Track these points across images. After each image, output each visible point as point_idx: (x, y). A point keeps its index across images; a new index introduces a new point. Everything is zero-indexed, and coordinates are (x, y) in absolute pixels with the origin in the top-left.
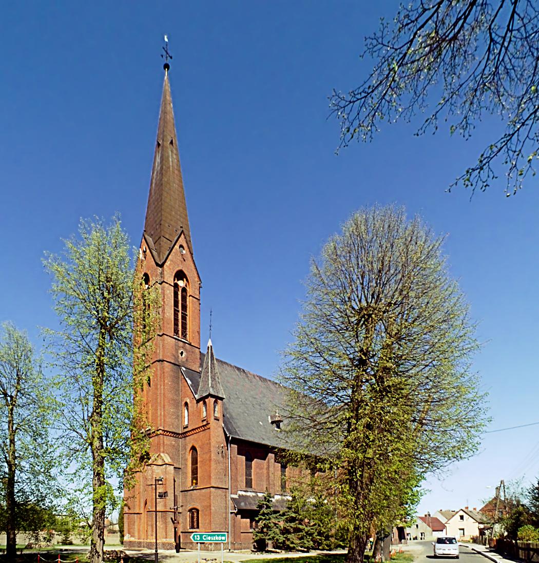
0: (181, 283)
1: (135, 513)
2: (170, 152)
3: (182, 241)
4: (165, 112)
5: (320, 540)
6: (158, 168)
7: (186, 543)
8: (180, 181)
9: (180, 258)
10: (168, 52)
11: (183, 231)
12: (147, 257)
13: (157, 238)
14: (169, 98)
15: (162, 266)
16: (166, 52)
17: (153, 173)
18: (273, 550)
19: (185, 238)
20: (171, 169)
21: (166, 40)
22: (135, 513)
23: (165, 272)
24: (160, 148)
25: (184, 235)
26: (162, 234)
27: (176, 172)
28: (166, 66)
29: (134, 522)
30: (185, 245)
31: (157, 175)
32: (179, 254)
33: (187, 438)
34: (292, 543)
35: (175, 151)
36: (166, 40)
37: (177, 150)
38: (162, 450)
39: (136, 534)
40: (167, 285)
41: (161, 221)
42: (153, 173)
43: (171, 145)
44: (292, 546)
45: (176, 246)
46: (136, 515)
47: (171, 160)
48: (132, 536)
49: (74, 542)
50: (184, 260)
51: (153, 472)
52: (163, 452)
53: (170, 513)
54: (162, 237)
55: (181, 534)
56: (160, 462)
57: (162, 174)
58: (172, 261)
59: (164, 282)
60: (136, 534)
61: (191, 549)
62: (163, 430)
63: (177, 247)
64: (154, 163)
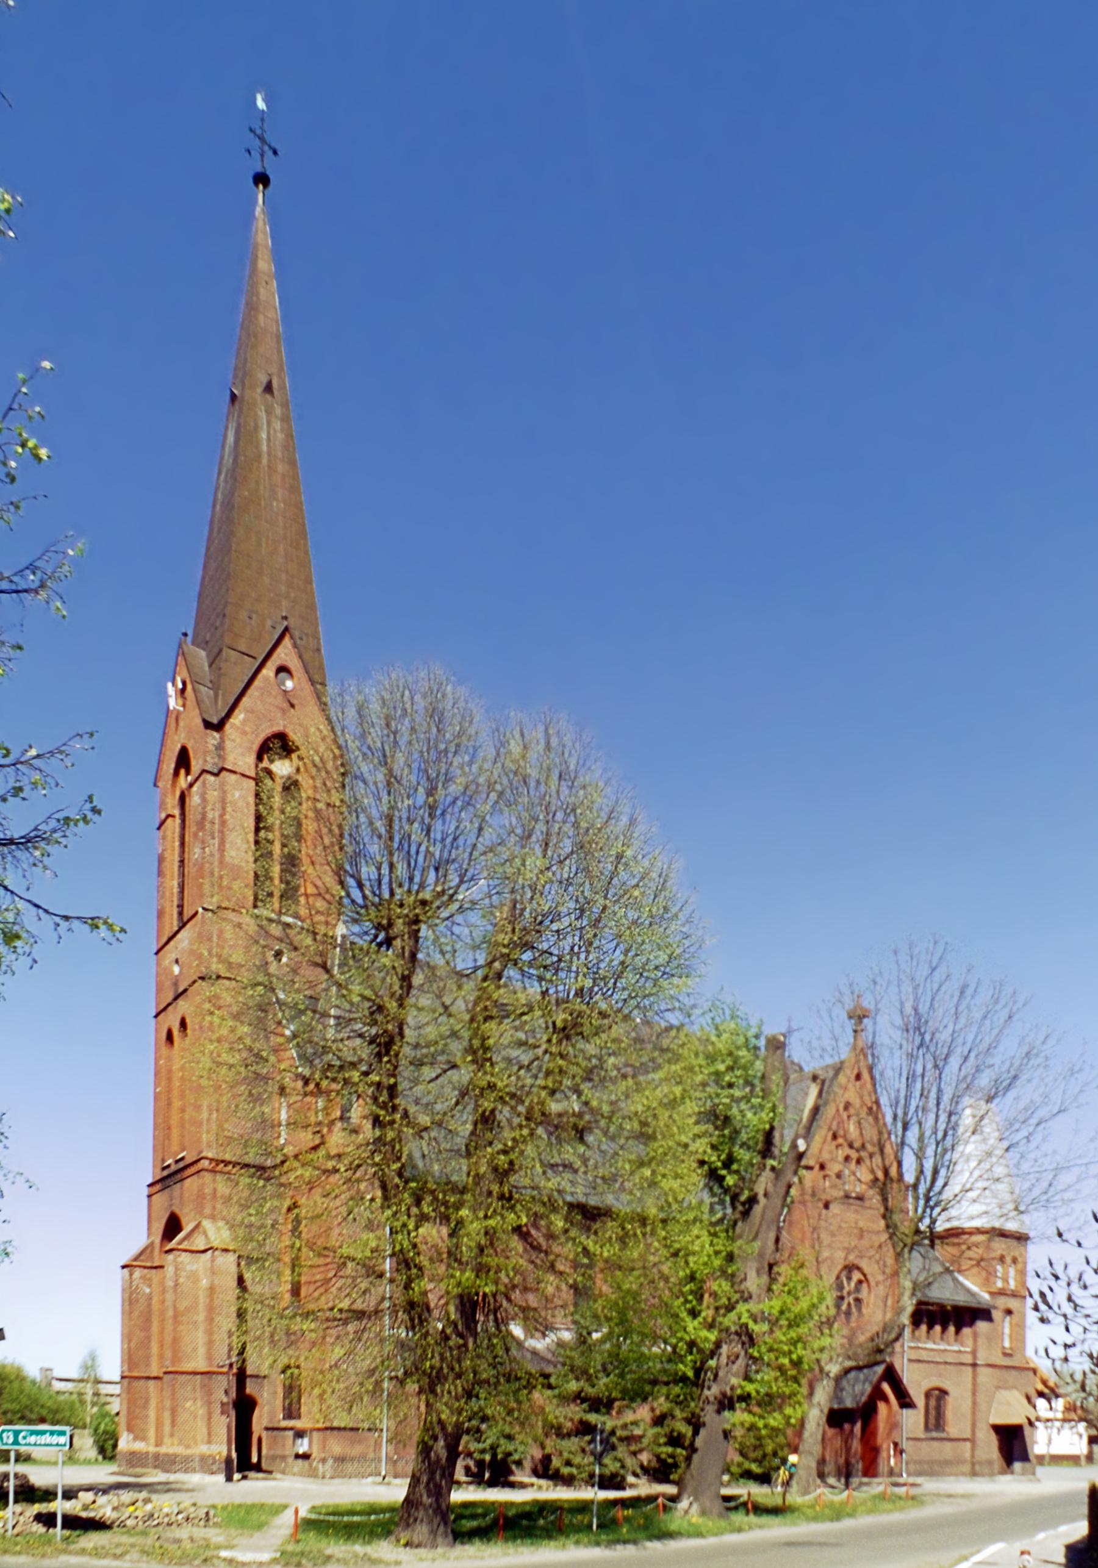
0: (282, 768)
1: (148, 1378)
2: (263, 415)
3: (285, 654)
4: (252, 308)
5: (672, 1456)
6: (228, 461)
7: (274, 1458)
8: (294, 489)
9: (280, 701)
10: (268, 137)
11: (286, 629)
12: (188, 703)
13: (216, 650)
14: (265, 264)
15: (219, 727)
16: (261, 139)
17: (219, 474)
18: (534, 1480)
19: (295, 646)
20: (265, 461)
21: (261, 104)
22: (148, 1378)
23: (228, 745)
24: (237, 404)
25: (291, 637)
26: (227, 640)
27: (281, 468)
28: (262, 179)
29: (147, 1401)
30: (294, 663)
31: (226, 481)
32: (275, 691)
33: (188, 1182)
34: (568, 1463)
35: (278, 411)
36: (261, 104)
37: (285, 405)
38: (207, 1211)
39: (152, 1434)
40: (233, 777)
41: (225, 606)
42: (219, 474)
43: (268, 397)
44: (566, 1471)
45: (264, 671)
46: (151, 1383)
47: (264, 436)
48: (136, 1438)
49: (37, 1453)
50: (292, 706)
51: (177, 1269)
52: (213, 1217)
53: (220, 1377)
54: (226, 652)
55: (264, 1434)
56: (200, 1243)
57: (235, 479)
58: (247, 711)
59: (223, 769)
60: (152, 1434)
61: (283, 1472)
62: (211, 1160)
63: (268, 672)
64: (223, 447)
